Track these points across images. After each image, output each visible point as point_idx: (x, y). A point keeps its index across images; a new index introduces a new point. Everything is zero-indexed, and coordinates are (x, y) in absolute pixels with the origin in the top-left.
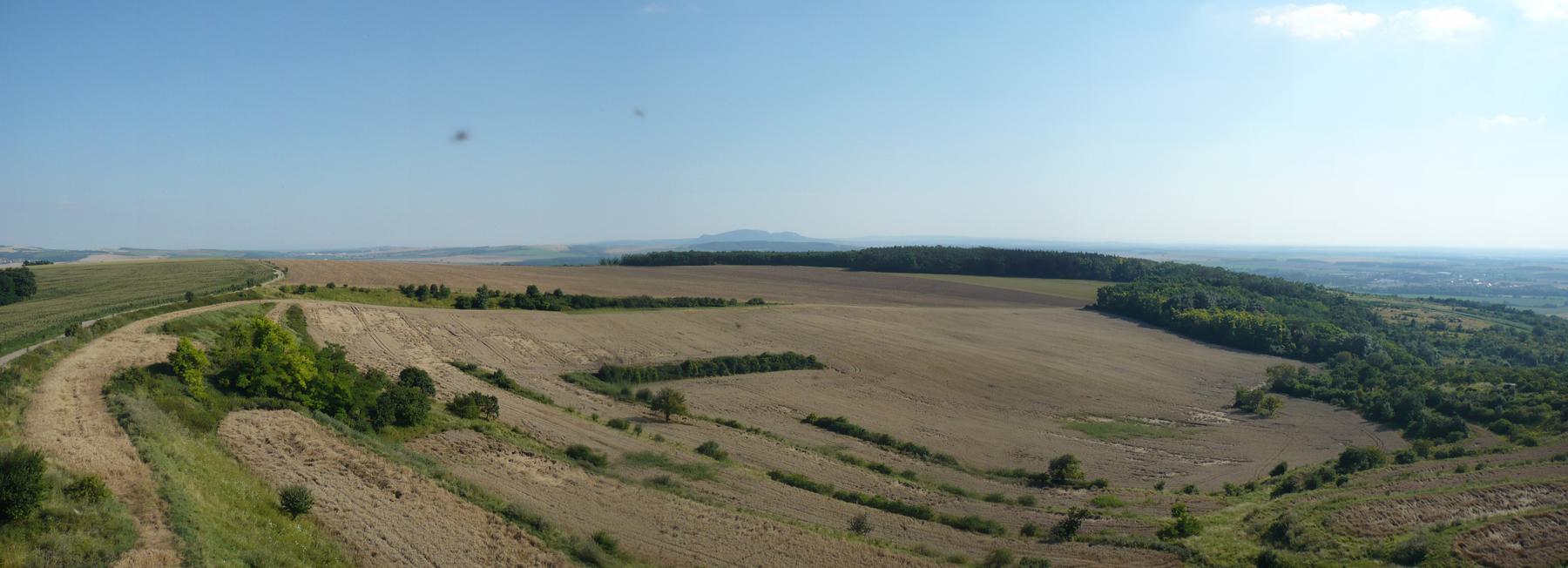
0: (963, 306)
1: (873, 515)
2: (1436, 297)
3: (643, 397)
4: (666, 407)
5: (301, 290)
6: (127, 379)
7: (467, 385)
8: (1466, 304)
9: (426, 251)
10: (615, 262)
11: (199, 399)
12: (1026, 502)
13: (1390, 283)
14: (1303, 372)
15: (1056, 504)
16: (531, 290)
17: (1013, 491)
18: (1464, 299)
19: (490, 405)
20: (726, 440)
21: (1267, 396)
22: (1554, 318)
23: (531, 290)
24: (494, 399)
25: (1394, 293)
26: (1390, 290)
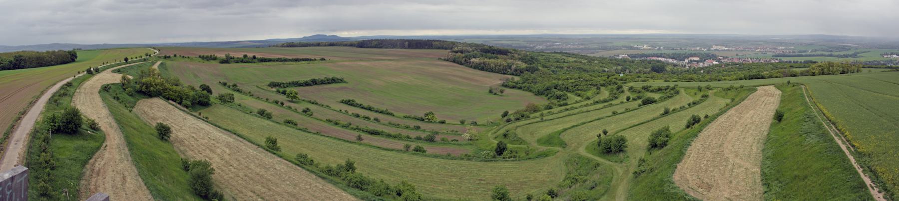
0: (369, 60)
1: (363, 135)
2: (556, 51)
3: (284, 93)
4: (293, 98)
5: (165, 57)
6: (106, 89)
7: (225, 91)
8: (566, 53)
9: (508, 38)
10: (351, 45)
11: (463, 157)
12: (418, 128)
13: (539, 47)
14: (513, 79)
15: (427, 128)
16: (245, 56)
17: (413, 123)
18: (565, 52)
19: (232, 98)
20: (312, 107)
21: (500, 88)
22: (594, 57)
23: (245, 56)
24: (233, 95)
25: (542, 51)
26: (542, 49)
